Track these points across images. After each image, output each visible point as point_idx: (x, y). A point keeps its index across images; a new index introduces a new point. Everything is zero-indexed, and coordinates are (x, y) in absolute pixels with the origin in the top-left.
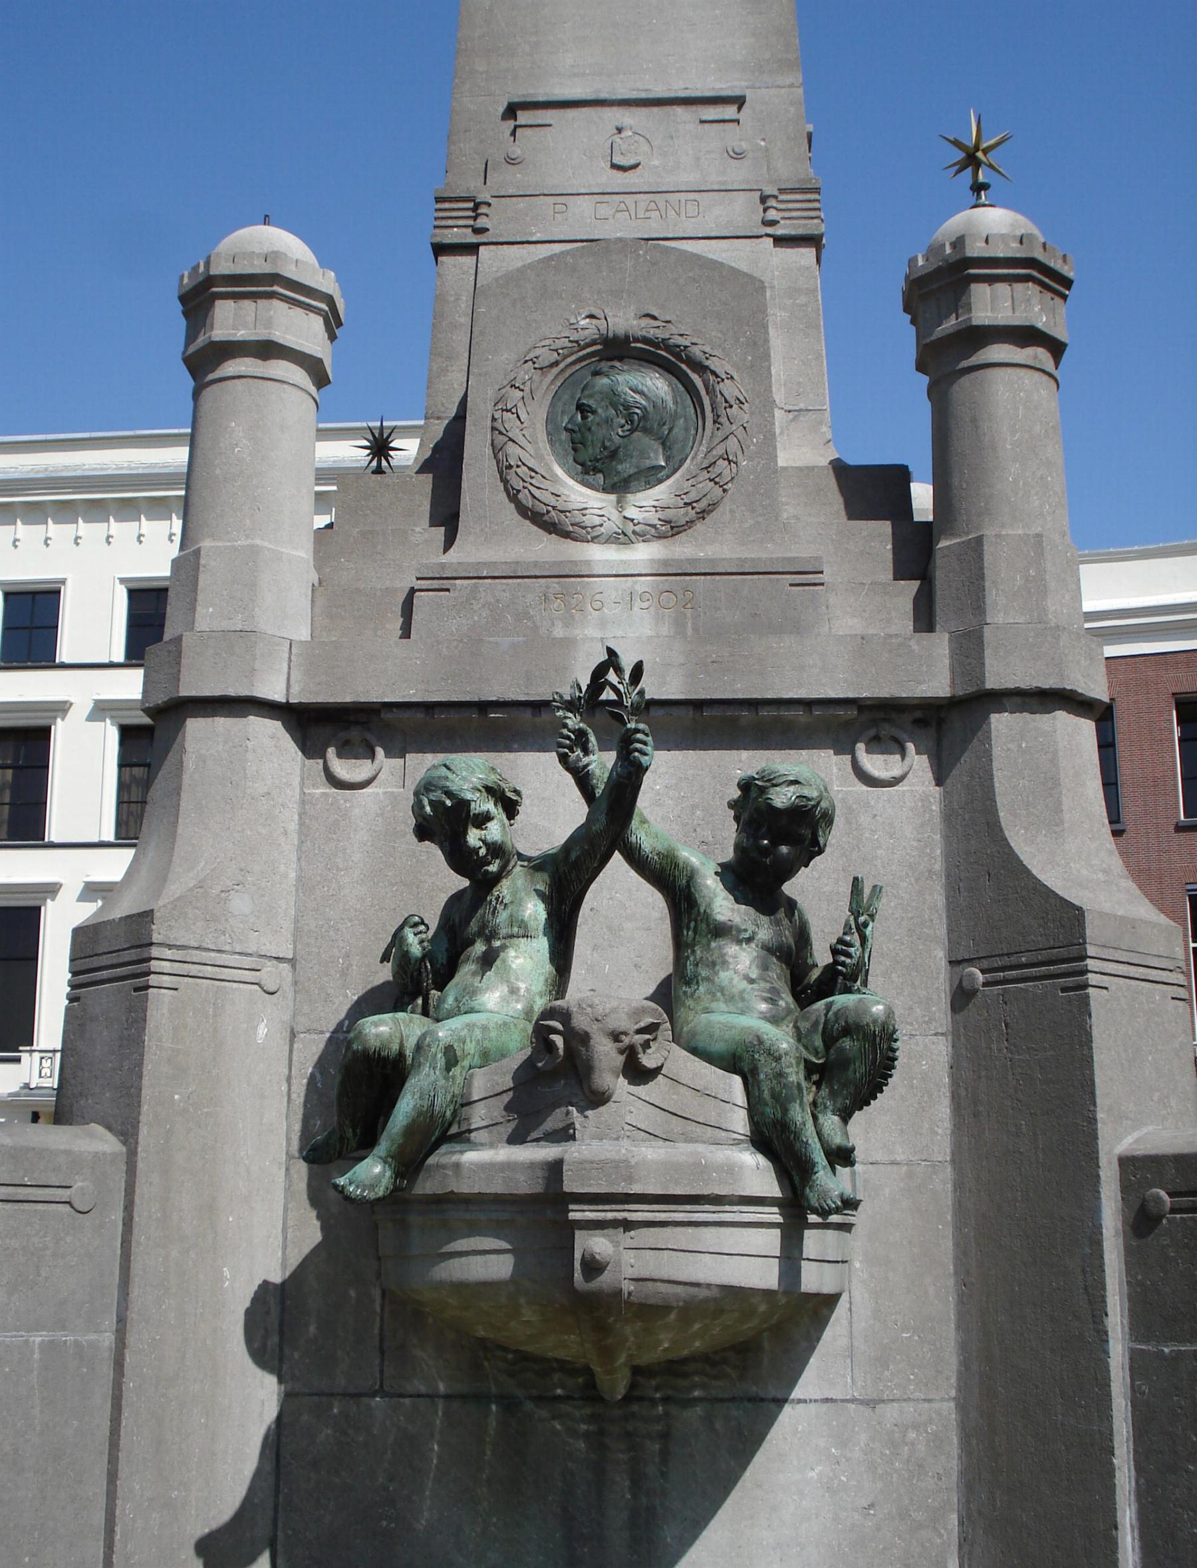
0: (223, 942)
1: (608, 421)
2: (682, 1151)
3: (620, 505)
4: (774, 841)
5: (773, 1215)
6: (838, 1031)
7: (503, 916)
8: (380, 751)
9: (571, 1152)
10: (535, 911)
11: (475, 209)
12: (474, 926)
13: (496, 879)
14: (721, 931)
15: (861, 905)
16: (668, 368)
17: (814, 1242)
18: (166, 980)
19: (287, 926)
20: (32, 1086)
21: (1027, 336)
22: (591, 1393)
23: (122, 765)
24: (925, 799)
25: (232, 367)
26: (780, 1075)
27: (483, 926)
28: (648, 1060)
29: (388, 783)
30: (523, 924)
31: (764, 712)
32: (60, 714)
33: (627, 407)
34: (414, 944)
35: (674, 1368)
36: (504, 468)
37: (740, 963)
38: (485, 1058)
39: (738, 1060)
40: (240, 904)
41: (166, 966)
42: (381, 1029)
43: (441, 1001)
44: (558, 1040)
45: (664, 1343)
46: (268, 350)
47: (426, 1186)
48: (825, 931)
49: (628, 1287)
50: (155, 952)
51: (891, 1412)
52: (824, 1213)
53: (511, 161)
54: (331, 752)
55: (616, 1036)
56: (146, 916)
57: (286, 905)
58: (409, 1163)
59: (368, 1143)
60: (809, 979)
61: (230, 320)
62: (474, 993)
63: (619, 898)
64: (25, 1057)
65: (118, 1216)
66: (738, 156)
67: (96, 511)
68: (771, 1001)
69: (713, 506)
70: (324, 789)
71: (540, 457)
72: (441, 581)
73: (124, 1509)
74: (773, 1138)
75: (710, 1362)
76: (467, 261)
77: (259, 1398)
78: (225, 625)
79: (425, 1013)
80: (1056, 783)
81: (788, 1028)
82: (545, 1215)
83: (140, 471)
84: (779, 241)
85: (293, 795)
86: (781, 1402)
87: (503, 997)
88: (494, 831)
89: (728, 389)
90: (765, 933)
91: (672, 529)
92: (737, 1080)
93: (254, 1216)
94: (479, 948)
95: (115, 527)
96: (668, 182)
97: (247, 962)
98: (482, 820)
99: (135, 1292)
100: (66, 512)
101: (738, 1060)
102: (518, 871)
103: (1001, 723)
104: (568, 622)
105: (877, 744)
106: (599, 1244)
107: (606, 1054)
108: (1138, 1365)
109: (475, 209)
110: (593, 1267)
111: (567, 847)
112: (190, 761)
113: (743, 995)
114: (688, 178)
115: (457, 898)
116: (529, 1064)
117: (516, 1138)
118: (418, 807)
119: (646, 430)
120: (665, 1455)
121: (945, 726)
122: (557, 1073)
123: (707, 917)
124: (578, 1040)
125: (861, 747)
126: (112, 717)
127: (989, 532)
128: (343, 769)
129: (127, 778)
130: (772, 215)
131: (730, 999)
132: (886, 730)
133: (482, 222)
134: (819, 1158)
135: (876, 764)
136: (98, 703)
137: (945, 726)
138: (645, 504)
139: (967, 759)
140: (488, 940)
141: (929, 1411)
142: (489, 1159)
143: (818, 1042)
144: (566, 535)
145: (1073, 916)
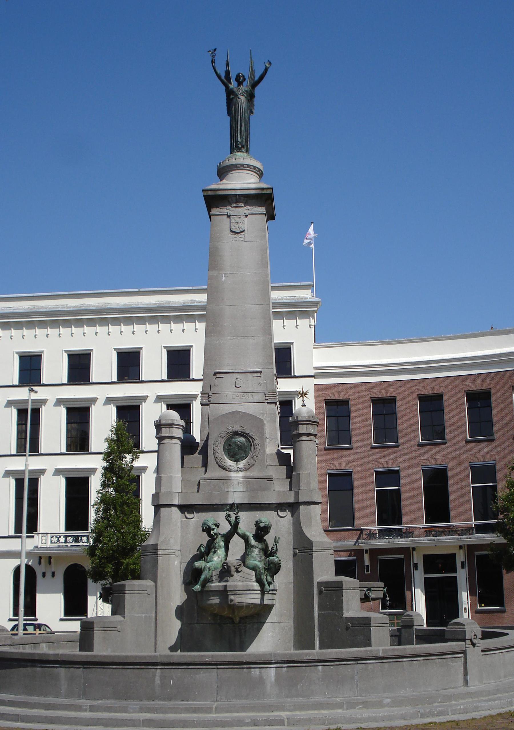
0: (169, 548)
1: (234, 448)
2: (245, 583)
3: (237, 464)
4: (262, 531)
5: (259, 592)
6: (271, 563)
7: (217, 545)
8: (195, 512)
9: (228, 584)
10: (222, 544)
11: (209, 396)
12: (212, 546)
13: (216, 538)
14: (253, 546)
15: (276, 541)
16: (245, 437)
17: (266, 596)
18: (161, 555)
19: (179, 544)
20: (39, 547)
21: (309, 435)
22: (233, 622)
23: (68, 423)
24: (290, 520)
25: (166, 441)
26: (260, 571)
27: (214, 546)
28: (239, 570)
29: (197, 519)
30: (220, 546)
31: (262, 505)
32: (43, 404)
33: (238, 445)
34: (202, 549)
35: (246, 617)
36: (215, 458)
37: (256, 551)
38: (215, 569)
39: (254, 568)
40: (172, 541)
41: (160, 553)
42: (198, 564)
43: (207, 559)
44: (226, 567)
45: (243, 613)
46: (172, 438)
47: (206, 589)
48: (271, 543)
49: (237, 604)
50: (159, 551)
51: (282, 624)
52: (268, 592)
53: (216, 385)
54: (186, 513)
55: (234, 566)
56: (157, 545)
57: (179, 541)
58: (203, 585)
59: (196, 583)
60: (267, 553)
61: (165, 432)
62: (213, 558)
63: (237, 543)
64: (36, 536)
65: (154, 595)
66: (260, 385)
67: (55, 324)
68: (260, 558)
69: (254, 465)
70: (185, 519)
71: (222, 455)
72: (205, 480)
73: (158, 642)
74: (259, 580)
75: (252, 617)
76: (207, 407)
77: (178, 624)
78: (167, 491)
79: (204, 561)
80: (311, 518)
81: (263, 563)
82: (224, 593)
83: (72, 309)
84: (268, 403)
85: (180, 520)
86: (265, 623)
87: (217, 559)
88: (215, 531)
89: (256, 442)
90: (260, 546)
91: (246, 469)
92: (254, 572)
93: (176, 595)
94: (213, 550)
95: (62, 330)
96: (246, 391)
97: (173, 551)
98: (213, 529)
99: (158, 607)
100: (43, 325)
101: (254, 568)
102: (219, 537)
103: (302, 507)
104: (227, 488)
105: (281, 510)
106: (232, 597)
107: (233, 569)
108: (319, 615)
109: (209, 396)
110: (232, 600)
111: (227, 533)
112: (162, 516)
113: (256, 558)
114: (250, 390)
115: (209, 541)
116: (221, 570)
117: (220, 582)
118: (203, 527)
119: (242, 450)
120: (245, 632)
121: (293, 507)
122: (225, 572)
123: (250, 544)
124: (229, 567)
125: (279, 511)
126: (63, 405)
127: (301, 472)
128: (188, 516)
129: (70, 428)
130: (267, 398)
131: (254, 558)
132: (284, 508)
133: (210, 399)
134: (266, 583)
135: (281, 514)
136: (58, 399)
137: (293, 507)
138: (242, 464)
139: (296, 513)
140: (215, 548)
141: (289, 624)
142: (216, 585)
143: (267, 565)
144: (227, 470)
145: (310, 542)
